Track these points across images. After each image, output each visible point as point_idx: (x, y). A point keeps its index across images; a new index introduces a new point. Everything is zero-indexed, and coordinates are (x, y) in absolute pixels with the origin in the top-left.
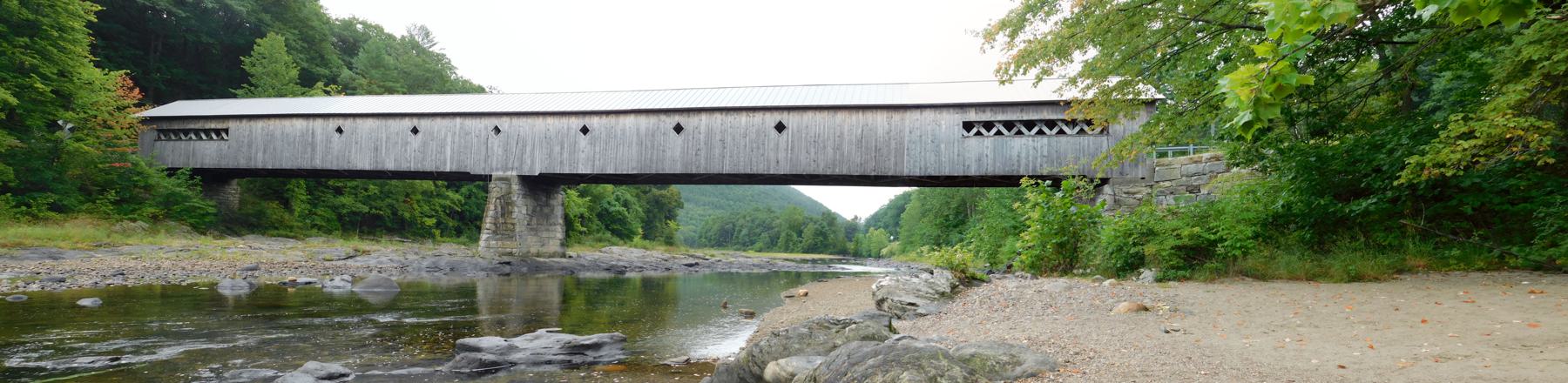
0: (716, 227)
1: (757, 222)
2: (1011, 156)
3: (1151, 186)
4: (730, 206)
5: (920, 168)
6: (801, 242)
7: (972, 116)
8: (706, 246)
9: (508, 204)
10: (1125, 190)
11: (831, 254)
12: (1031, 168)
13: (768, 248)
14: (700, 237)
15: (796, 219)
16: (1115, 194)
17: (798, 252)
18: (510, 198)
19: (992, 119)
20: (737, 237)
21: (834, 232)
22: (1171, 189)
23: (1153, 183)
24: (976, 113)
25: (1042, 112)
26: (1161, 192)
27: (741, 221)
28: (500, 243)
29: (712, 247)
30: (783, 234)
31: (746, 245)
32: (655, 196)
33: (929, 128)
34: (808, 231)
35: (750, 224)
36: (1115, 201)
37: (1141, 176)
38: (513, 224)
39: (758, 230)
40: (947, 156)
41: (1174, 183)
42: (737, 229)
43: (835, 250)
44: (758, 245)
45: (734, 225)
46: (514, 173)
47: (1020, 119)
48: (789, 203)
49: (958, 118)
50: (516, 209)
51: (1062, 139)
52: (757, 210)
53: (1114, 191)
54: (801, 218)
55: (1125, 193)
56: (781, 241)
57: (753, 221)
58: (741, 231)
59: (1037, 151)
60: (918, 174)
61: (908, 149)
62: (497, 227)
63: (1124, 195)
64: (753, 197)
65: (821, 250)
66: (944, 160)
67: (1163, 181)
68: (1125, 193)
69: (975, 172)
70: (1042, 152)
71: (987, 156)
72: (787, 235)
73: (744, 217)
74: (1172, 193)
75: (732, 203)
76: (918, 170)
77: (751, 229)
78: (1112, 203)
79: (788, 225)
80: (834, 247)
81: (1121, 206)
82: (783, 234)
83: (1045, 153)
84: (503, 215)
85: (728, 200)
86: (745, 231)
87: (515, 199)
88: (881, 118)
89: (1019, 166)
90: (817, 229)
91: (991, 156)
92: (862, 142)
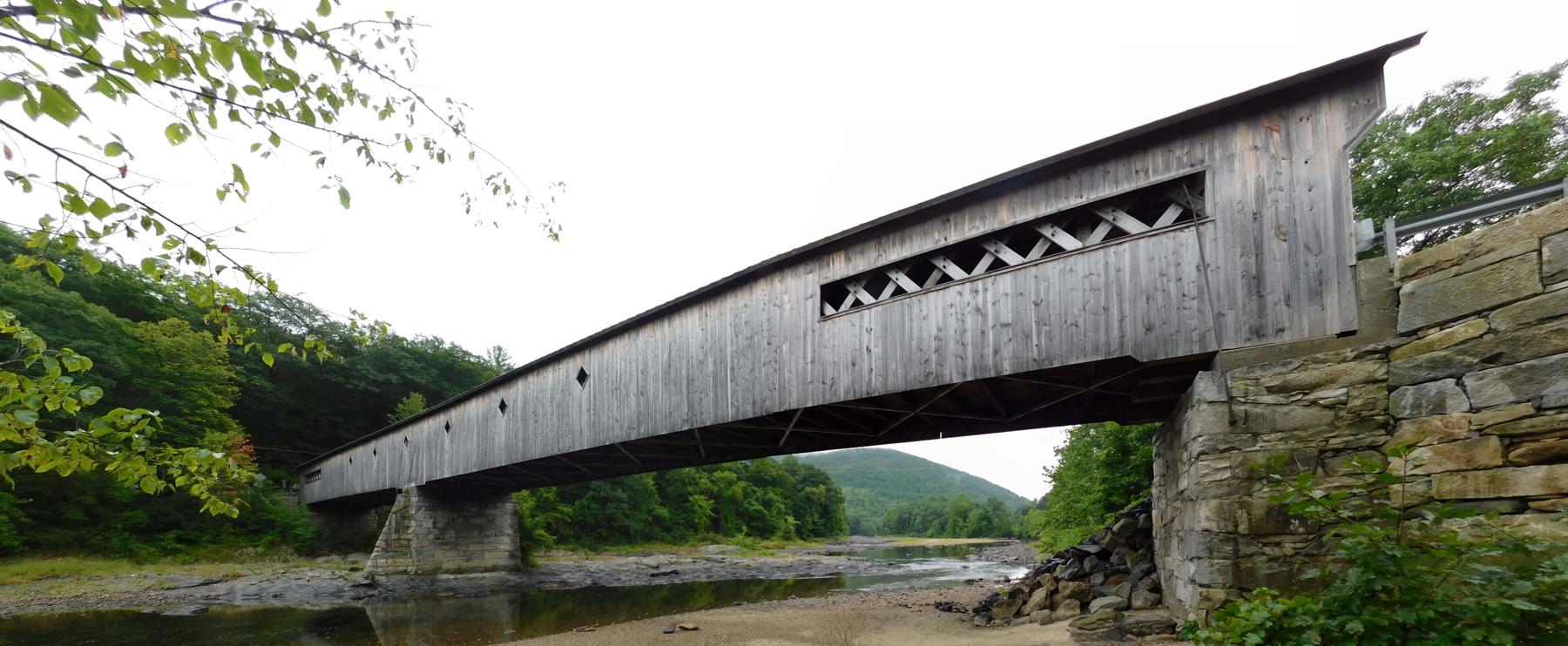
0: (895, 517)
1: (930, 511)
2: (920, 338)
3: (1386, 354)
4: (921, 497)
5: (754, 403)
6: (967, 527)
7: (839, 268)
8: (888, 534)
9: (404, 518)
10: (1270, 379)
11: (996, 537)
12: (970, 364)
13: (939, 533)
14: (884, 526)
15: (963, 506)
16: (1231, 399)
17: (964, 537)
18: (408, 511)
19: (882, 262)
20: (913, 525)
21: (999, 516)
22: (1489, 345)
23: (1392, 342)
24: (848, 260)
25: (995, 213)
26: (1434, 364)
27: (916, 511)
28: (390, 561)
29: (893, 534)
30: (950, 521)
31: (921, 532)
32: (806, 493)
33: (764, 317)
34: (974, 515)
35: (923, 513)
36: (1233, 423)
37: (1335, 327)
38: (409, 540)
39: (930, 518)
40: (793, 369)
41: (1500, 321)
42: (912, 518)
43: (1000, 533)
44: (930, 531)
45: (911, 515)
46: (413, 485)
47: (942, 243)
48: (976, 491)
49: (806, 284)
50: (413, 523)
51: (1053, 268)
52: (933, 499)
53: (1228, 389)
54: (967, 504)
55: (1270, 390)
56: (949, 527)
57: (926, 510)
58: (916, 519)
59: (985, 316)
60: (750, 415)
61: (733, 369)
62: (388, 544)
63: (1270, 399)
64: (942, 488)
65: (985, 534)
66: (787, 375)
67: (1442, 325)
68: (1270, 390)
69: (846, 392)
70: (997, 315)
71: (869, 350)
72: (954, 520)
73: (919, 507)
74: (1493, 360)
75: (923, 495)
76: (749, 408)
77: (924, 517)
78: (1221, 427)
79: (954, 512)
80: (999, 530)
81: (1256, 435)
82: (950, 521)
83: (1007, 317)
84: (397, 531)
85: (919, 492)
86: (919, 519)
87: (413, 512)
88: (691, 324)
89: (940, 364)
90: (981, 514)
91: (877, 350)
92: (669, 374)
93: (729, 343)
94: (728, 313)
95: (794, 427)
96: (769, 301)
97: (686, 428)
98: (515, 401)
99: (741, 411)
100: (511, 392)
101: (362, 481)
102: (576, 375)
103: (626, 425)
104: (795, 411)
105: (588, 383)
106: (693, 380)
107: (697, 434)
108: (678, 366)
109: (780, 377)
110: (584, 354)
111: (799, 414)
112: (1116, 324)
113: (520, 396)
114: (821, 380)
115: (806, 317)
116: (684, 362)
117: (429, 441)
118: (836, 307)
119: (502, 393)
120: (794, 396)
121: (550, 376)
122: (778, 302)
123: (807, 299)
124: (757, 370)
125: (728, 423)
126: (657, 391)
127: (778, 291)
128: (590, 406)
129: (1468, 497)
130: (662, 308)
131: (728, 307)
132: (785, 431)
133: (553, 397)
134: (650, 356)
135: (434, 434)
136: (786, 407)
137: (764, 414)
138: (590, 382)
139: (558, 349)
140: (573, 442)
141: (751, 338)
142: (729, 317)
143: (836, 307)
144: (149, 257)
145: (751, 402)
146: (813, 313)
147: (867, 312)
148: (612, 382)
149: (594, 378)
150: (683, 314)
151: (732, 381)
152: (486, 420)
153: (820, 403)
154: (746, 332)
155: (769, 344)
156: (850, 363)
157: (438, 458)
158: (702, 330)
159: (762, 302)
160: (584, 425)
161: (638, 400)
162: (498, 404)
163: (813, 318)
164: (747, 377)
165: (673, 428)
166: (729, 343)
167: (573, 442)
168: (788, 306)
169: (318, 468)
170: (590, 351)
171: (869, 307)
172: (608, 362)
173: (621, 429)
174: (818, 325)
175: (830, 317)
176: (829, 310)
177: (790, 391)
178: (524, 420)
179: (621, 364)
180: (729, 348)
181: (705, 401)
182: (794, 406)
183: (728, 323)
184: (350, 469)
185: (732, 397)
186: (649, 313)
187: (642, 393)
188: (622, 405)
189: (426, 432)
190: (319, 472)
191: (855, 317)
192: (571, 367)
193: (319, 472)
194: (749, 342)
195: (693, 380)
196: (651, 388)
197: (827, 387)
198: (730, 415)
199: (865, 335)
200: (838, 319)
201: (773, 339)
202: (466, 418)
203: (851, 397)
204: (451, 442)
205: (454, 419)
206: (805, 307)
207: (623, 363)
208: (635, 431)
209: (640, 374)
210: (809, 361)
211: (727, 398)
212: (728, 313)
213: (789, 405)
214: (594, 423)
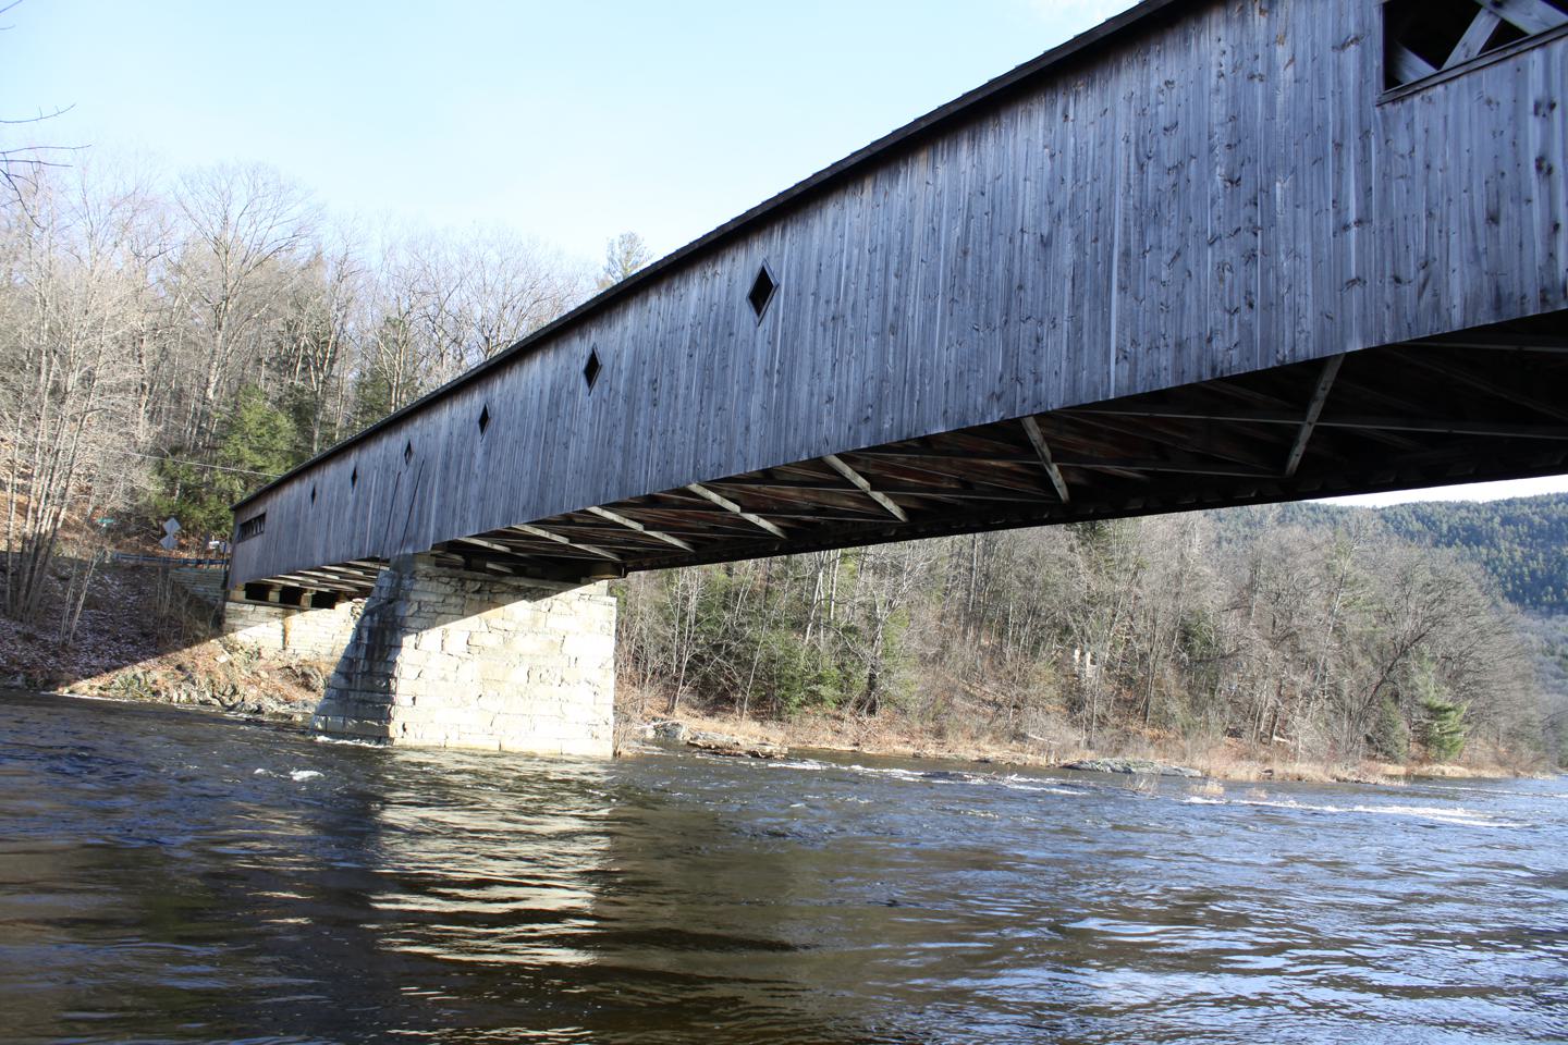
40: (1305, 246)
60: (1167, 381)
61: (1126, 254)
66: (1286, 264)
69: (1470, 304)
76: (1165, 359)
93: (1120, 189)
94: (1121, 109)
95: (1324, 415)
96: (1235, 69)
97: (995, 416)
98: (618, 356)
99: (1143, 368)
100: (611, 337)
101: (327, 539)
102: (748, 288)
103: (850, 411)
104: (1315, 366)
105: (772, 305)
106: (1020, 287)
107: (1035, 434)
108: (985, 254)
109: (1265, 273)
110: (771, 234)
111: (1327, 380)
112: (113, 1015)
113: (628, 344)
114: (1388, 273)
115: (1340, 95)
116: (1001, 244)
117: (448, 454)
118: (1437, 58)
119: (593, 339)
120: (1308, 323)
121: (694, 291)
122: (1260, 68)
123: (1342, 46)
124: (1192, 254)
125: (1107, 404)
126: (931, 318)
127: (1260, 38)
128: (772, 363)
129: (423, 392)
130: (953, 109)
131: (1122, 93)
132: (1297, 430)
133: (694, 343)
134: (919, 228)
135: (459, 435)
136: (1284, 354)
137: (1207, 377)
138: (778, 302)
139: (712, 228)
140: (729, 454)
141: (1178, 167)
142: (1124, 123)
143: (1437, 58)
144: (1552, 492)
145: (1171, 342)
146: (1361, 86)
147: (1537, 56)
148: (828, 302)
149: (787, 294)
150: (1005, 120)
151: (1123, 289)
152: (556, 399)
153: (1387, 340)
154: (1170, 149)
155: (1234, 182)
156: (1481, 217)
157: (460, 488)
158: (1052, 156)
159: (1214, 71)
160: (755, 409)
161: (884, 344)
162: (583, 364)
163: (1361, 98)
164: (1164, 275)
165: (964, 419)
166: (1120, 189)
167: (729, 454)
168: (1286, 75)
169: (261, 510)
170: (784, 228)
171: (1545, 39)
172: (821, 251)
173: (839, 420)
174: (1377, 111)
175: (1421, 86)
176: (1416, 67)
177: (1296, 310)
178: (630, 399)
179: (850, 255)
180: (1119, 199)
181: (1049, 341)
182: (1307, 350)
183: (1120, 135)
184: (310, 511)
185: (1121, 330)
186: (923, 125)
187: (892, 327)
188: (847, 357)
189: (444, 433)
190: (262, 517)
191: (1495, 80)
192: (738, 269)
193: (262, 517)
194: (1172, 178)
195: (1020, 287)
196: (915, 310)
197: (1409, 291)
198: (1115, 380)
199: (1533, 127)
200: (1440, 88)
201: (1247, 166)
202: (520, 397)
203: (1485, 318)
204: (487, 453)
205: (496, 403)
206: (1339, 68)
207: (856, 251)
208: (870, 427)
209: (893, 279)
210: (1352, 217)
211: (1108, 334)
212: (1121, 109)
213: (1293, 350)
214: (778, 407)
